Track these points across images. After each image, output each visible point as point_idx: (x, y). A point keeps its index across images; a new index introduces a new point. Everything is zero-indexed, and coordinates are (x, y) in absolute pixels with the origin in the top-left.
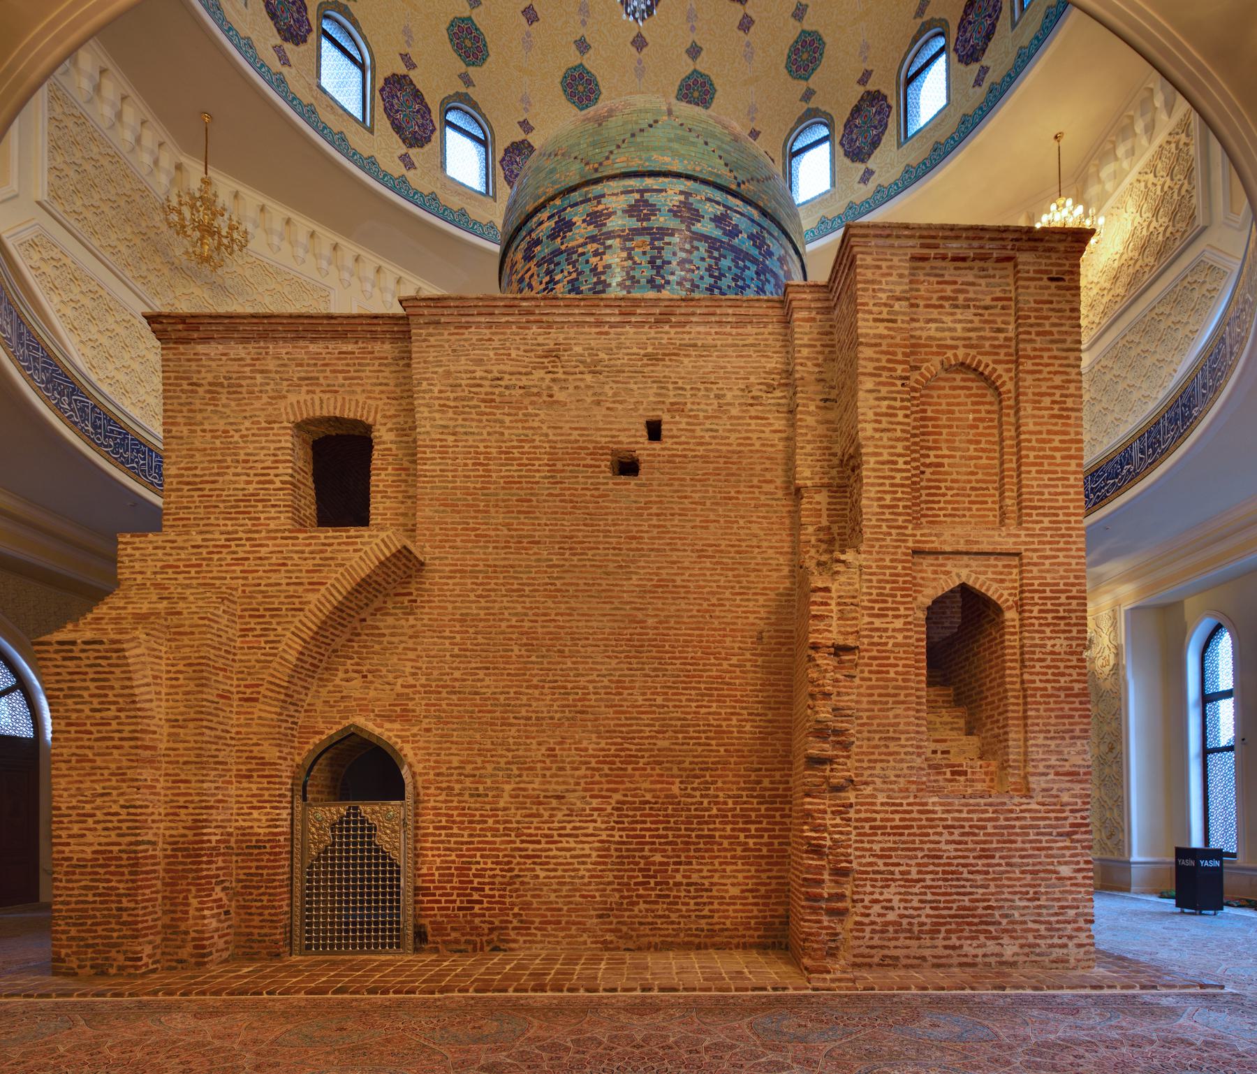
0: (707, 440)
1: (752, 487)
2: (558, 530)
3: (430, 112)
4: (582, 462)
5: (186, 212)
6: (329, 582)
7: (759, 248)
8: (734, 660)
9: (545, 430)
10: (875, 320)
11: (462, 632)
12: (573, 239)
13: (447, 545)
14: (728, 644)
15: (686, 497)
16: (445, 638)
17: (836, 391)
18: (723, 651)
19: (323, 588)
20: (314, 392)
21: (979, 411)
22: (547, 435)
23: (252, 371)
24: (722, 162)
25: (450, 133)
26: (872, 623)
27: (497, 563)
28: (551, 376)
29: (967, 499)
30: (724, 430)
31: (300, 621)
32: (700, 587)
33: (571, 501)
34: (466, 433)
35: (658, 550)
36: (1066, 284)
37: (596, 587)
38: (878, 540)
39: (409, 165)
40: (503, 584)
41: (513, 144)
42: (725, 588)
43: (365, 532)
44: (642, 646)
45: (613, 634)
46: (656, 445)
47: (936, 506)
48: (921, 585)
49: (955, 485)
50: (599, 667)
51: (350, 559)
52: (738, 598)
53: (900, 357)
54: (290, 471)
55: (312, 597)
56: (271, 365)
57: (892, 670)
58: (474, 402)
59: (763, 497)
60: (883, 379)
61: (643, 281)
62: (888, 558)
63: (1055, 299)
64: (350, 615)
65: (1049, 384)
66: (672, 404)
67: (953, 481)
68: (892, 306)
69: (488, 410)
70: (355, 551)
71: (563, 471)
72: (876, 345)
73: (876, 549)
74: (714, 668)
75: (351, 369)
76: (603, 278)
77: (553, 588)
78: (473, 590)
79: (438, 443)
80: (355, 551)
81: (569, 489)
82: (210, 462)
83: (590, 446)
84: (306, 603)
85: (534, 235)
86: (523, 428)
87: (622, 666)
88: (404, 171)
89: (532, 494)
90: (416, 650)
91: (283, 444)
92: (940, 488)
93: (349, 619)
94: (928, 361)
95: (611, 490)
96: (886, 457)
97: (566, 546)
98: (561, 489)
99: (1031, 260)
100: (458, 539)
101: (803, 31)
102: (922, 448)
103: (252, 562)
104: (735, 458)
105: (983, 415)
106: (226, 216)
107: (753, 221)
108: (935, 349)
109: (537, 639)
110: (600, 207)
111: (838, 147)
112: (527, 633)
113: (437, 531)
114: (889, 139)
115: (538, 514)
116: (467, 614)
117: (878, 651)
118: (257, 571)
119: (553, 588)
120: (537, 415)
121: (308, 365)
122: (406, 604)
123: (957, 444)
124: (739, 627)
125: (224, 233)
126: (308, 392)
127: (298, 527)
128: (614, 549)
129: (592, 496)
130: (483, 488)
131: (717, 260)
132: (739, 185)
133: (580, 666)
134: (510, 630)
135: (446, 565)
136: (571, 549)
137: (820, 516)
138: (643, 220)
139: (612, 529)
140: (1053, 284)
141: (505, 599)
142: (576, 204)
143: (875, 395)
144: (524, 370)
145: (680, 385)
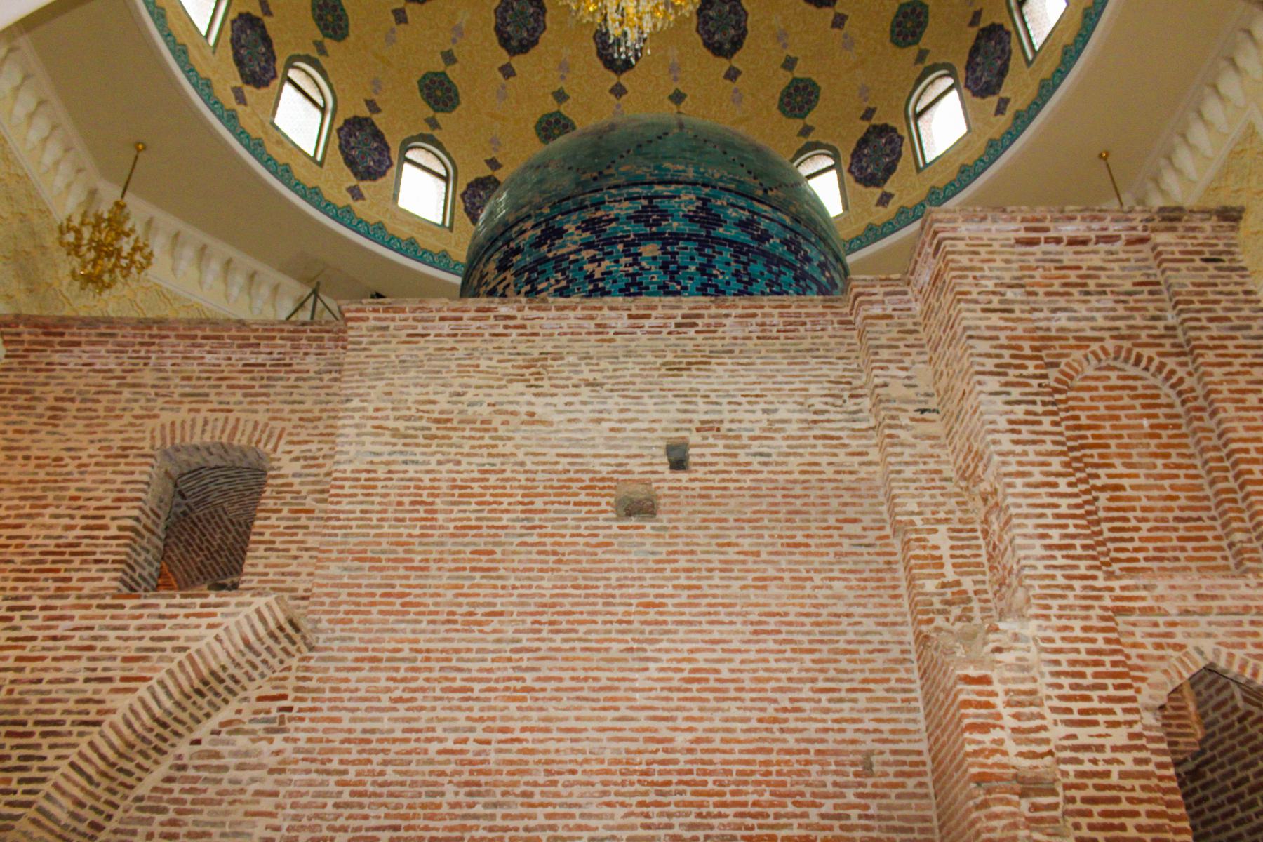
0: (756, 467)
1: (828, 528)
2: (533, 595)
3: (388, 149)
4: (573, 499)
5: (86, 233)
6: (157, 676)
7: (796, 253)
8: (828, 806)
9: (521, 457)
10: (984, 310)
11: (360, 762)
12: (563, 246)
13: (356, 618)
14: (814, 777)
15: (729, 545)
16: (328, 772)
17: (936, 399)
18: (808, 790)
19: (142, 689)
20: (198, 411)
21: (1155, 416)
22: (522, 464)
23: (119, 385)
24: (744, 170)
25: (288, 88)
26: (1074, 736)
27: (431, 646)
28: (534, 390)
29: (1174, 535)
30: (779, 454)
31: (92, 745)
32: (759, 680)
33: (555, 553)
34: (405, 462)
35: (690, 623)
36: (1226, 264)
37: (591, 683)
38: (1053, 596)
39: (241, 99)
40: (438, 680)
41: (375, 179)
42: (801, 680)
43: (232, 599)
44: (668, 783)
45: (618, 762)
46: (683, 476)
47: (1129, 545)
48: (1141, 669)
49: (1150, 515)
50: (592, 823)
51: (197, 639)
52: (824, 697)
53: (1028, 352)
54: (136, 513)
55: (122, 703)
56: (148, 377)
57: (1130, 822)
58: (424, 423)
59: (846, 541)
60: (1010, 379)
61: (653, 287)
62: (1077, 624)
63: (1218, 281)
64: (176, 733)
65: (1248, 378)
66: (703, 422)
67: (1144, 509)
68: (1003, 295)
69: (440, 433)
70: (211, 626)
71: (544, 511)
72: (991, 338)
73: (1055, 611)
74: (795, 822)
75: (256, 383)
76: (601, 285)
77: (519, 685)
78: (388, 690)
79: (364, 475)
80: (211, 626)
81: (553, 535)
82: (22, 498)
83: (586, 477)
84: (107, 712)
85: (513, 245)
86: (490, 455)
87: (632, 820)
88: (350, 201)
89: (495, 544)
90: (276, 794)
91: (136, 477)
92: (1126, 520)
93: (173, 739)
94: (1066, 356)
95: (616, 536)
96: (1038, 478)
97: (544, 618)
98: (540, 536)
99: (1019, 298)
100: (375, 609)
102: (1087, 465)
103: (39, 643)
104: (798, 490)
105: (1162, 420)
106: (133, 237)
107: (785, 226)
108: (1072, 342)
109: (488, 773)
110: (599, 214)
111: (964, 91)
112: (471, 763)
113: (343, 597)
114: (1016, 62)
115: (502, 572)
116: (373, 731)
117: (1097, 787)
118: (42, 659)
119: (519, 685)
120: (510, 439)
121: (199, 379)
122: (275, 714)
123: (1135, 460)
124: (831, 746)
125: (124, 254)
126: (190, 410)
127: (125, 590)
128: (620, 622)
129: (587, 544)
130: (422, 535)
131: (746, 265)
132: (765, 191)
133: (560, 823)
134: (443, 757)
135: (350, 650)
136: (551, 623)
137: (942, 566)
138: (651, 226)
139: (617, 592)
140: (1210, 266)
141: (439, 704)
142: (569, 212)
143: (1004, 398)
144: (496, 383)
145: (713, 399)
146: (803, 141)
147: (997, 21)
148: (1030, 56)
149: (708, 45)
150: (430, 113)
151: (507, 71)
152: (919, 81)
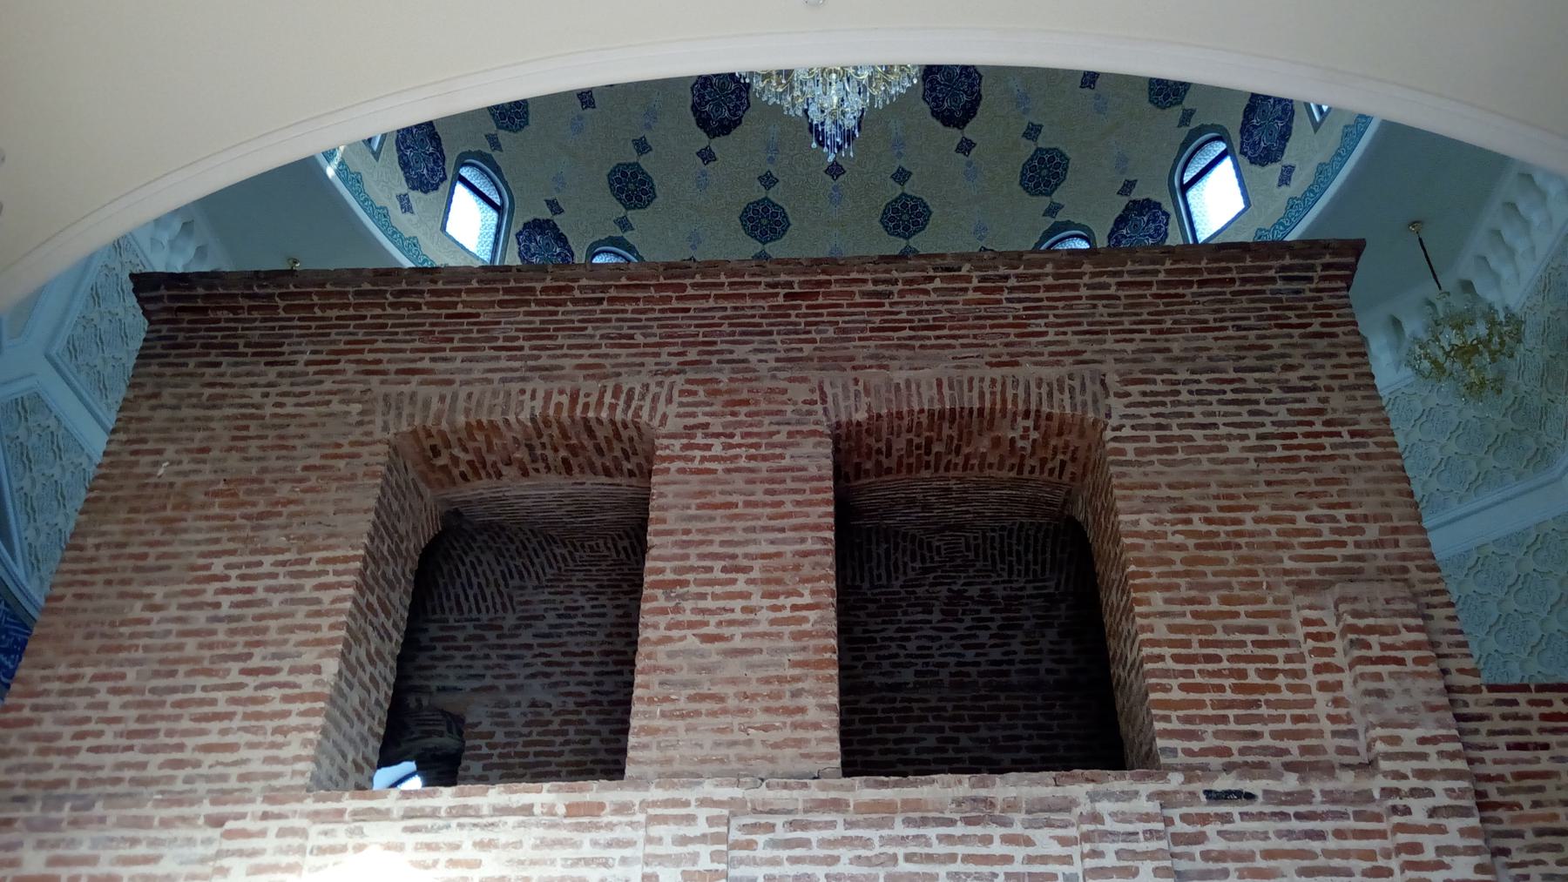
25: (460, 189)
39: (406, 207)
101: (1038, 149)
111: (1240, 158)
146: (1049, 222)
147: (1155, 198)
148: (1318, 118)
149: (935, 114)
150: (620, 211)
151: (707, 156)
152: (1185, 145)
